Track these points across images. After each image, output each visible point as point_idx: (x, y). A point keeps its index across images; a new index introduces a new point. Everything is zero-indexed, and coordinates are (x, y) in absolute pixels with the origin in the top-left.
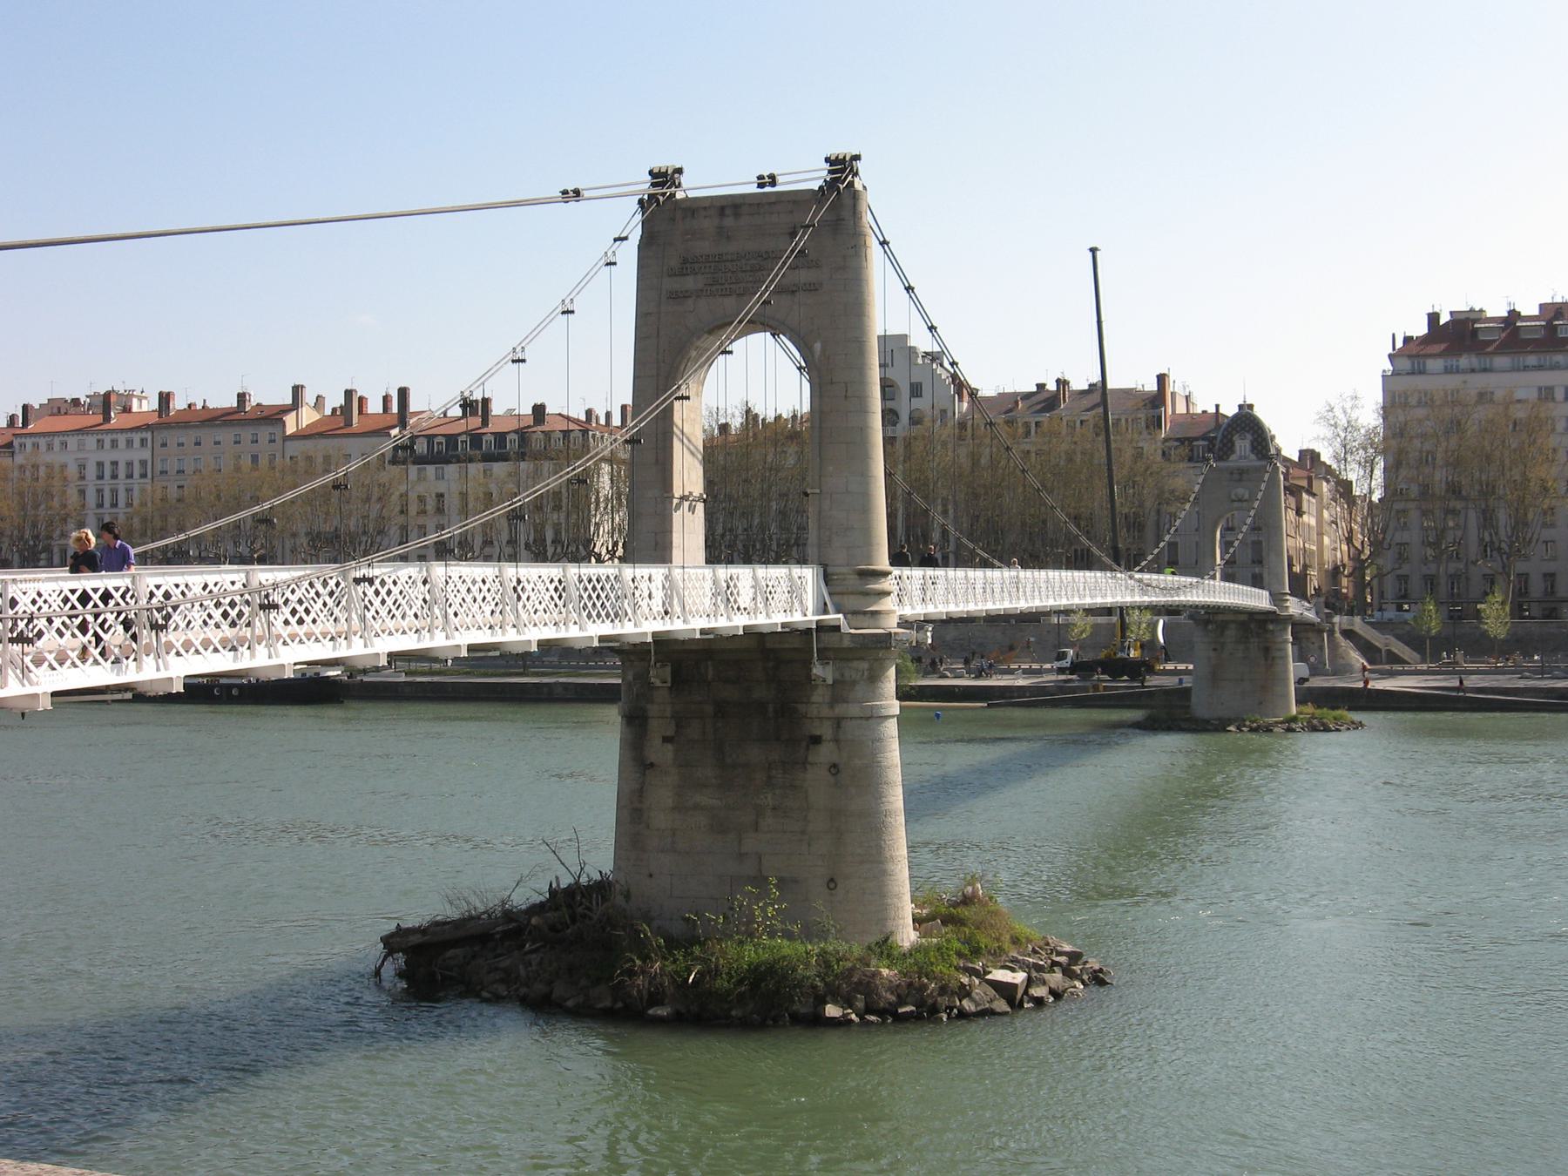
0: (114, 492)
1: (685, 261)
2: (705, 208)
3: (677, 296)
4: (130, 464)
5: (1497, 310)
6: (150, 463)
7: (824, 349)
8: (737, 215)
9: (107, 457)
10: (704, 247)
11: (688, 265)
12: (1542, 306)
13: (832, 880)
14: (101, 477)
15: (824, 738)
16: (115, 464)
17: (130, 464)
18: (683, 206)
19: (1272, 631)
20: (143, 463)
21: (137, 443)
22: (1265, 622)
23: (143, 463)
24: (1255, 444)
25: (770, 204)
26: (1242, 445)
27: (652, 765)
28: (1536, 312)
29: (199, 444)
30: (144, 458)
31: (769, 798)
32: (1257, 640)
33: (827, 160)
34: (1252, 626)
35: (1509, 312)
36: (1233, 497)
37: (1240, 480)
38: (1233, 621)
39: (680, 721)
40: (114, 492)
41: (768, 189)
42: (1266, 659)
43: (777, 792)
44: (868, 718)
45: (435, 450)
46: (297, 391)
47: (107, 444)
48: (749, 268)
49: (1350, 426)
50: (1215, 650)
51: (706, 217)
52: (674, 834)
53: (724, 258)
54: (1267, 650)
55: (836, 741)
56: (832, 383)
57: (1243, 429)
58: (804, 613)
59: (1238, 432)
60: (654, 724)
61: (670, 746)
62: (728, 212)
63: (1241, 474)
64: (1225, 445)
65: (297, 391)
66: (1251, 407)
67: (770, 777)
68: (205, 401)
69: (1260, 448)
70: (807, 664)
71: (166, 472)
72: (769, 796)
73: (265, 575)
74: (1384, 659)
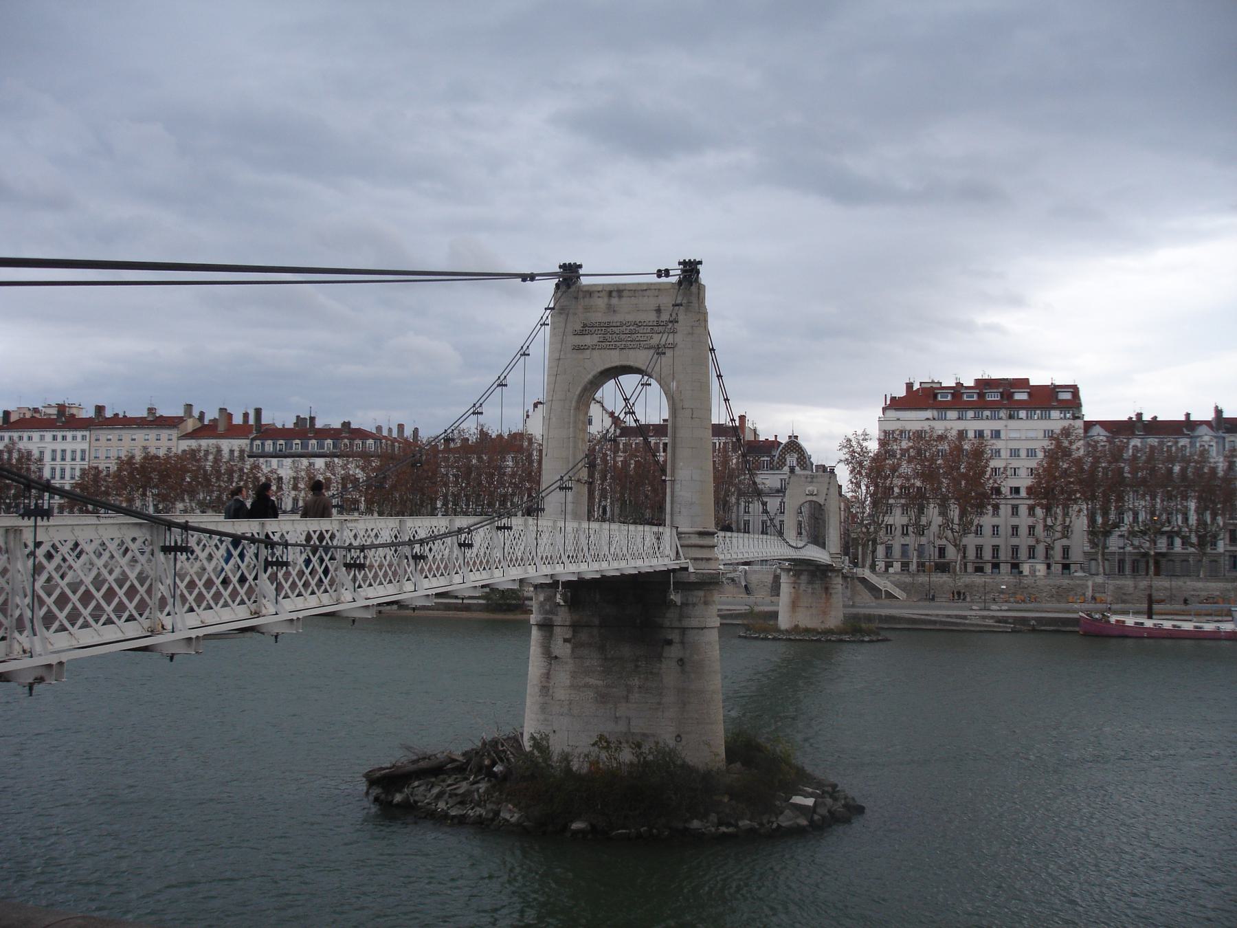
0: (63, 470)
1: (585, 326)
2: (599, 292)
3: (579, 348)
4: (74, 452)
5: (949, 382)
6: (87, 453)
7: (677, 387)
8: (620, 297)
9: (59, 446)
10: (598, 317)
11: (587, 328)
12: (977, 381)
13: (679, 736)
14: (54, 459)
15: (674, 640)
16: (64, 451)
17: (74, 452)
18: (584, 289)
19: (831, 576)
20: (83, 451)
21: (79, 439)
22: (826, 571)
23: (83, 451)
24: (799, 460)
25: (642, 290)
26: (792, 459)
27: (556, 657)
28: (972, 384)
29: (121, 440)
30: (84, 448)
31: (636, 680)
32: (820, 582)
33: (680, 263)
34: (818, 573)
35: (957, 383)
36: (807, 493)
37: (811, 482)
38: (805, 570)
39: (575, 627)
40: (63, 470)
41: (663, 279)
42: (826, 594)
43: (642, 676)
44: (702, 629)
45: (278, 449)
46: (189, 407)
47: (59, 438)
48: (627, 332)
49: (864, 452)
50: (794, 588)
51: (599, 297)
52: (570, 703)
53: (611, 325)
54: (827, 589)
55: (682, 643)
56: (683, 409)
57: (792, 451)
58: (662, 561)
59: (788, 453)
60: (557, 630)
61: (568, 645)
62: (614, 294)
63: (812, 478)
64: (781, 460)
65: (189, 407)
66: (796, 437)
67: (637, 666)
68: (125, 412)
69: (802, 463)
70: (665, 591)
71: (98, 457)
72: (636, 679)
73: (421, 526)
74: (883, 596)
